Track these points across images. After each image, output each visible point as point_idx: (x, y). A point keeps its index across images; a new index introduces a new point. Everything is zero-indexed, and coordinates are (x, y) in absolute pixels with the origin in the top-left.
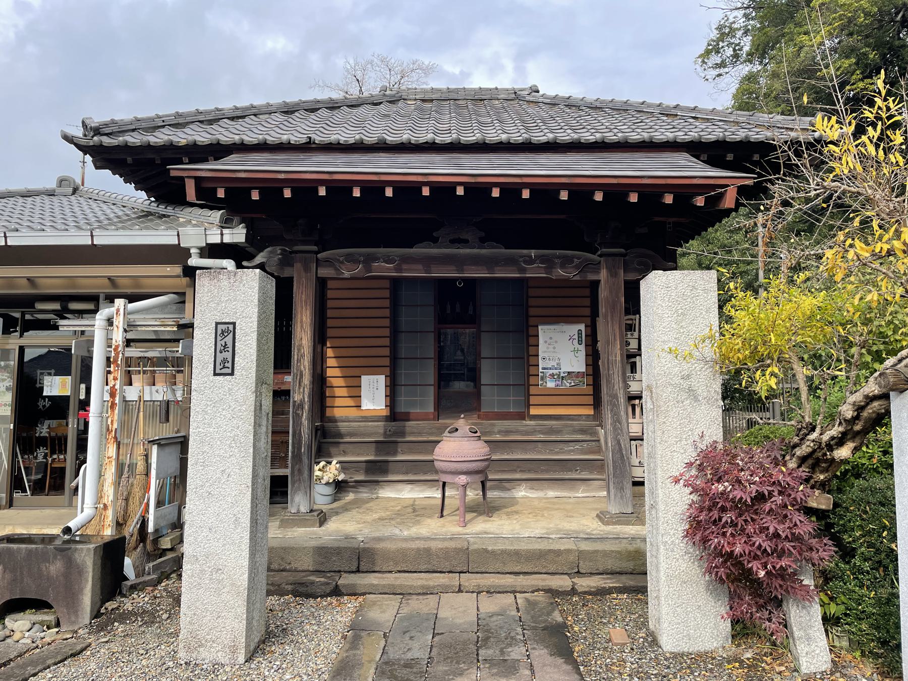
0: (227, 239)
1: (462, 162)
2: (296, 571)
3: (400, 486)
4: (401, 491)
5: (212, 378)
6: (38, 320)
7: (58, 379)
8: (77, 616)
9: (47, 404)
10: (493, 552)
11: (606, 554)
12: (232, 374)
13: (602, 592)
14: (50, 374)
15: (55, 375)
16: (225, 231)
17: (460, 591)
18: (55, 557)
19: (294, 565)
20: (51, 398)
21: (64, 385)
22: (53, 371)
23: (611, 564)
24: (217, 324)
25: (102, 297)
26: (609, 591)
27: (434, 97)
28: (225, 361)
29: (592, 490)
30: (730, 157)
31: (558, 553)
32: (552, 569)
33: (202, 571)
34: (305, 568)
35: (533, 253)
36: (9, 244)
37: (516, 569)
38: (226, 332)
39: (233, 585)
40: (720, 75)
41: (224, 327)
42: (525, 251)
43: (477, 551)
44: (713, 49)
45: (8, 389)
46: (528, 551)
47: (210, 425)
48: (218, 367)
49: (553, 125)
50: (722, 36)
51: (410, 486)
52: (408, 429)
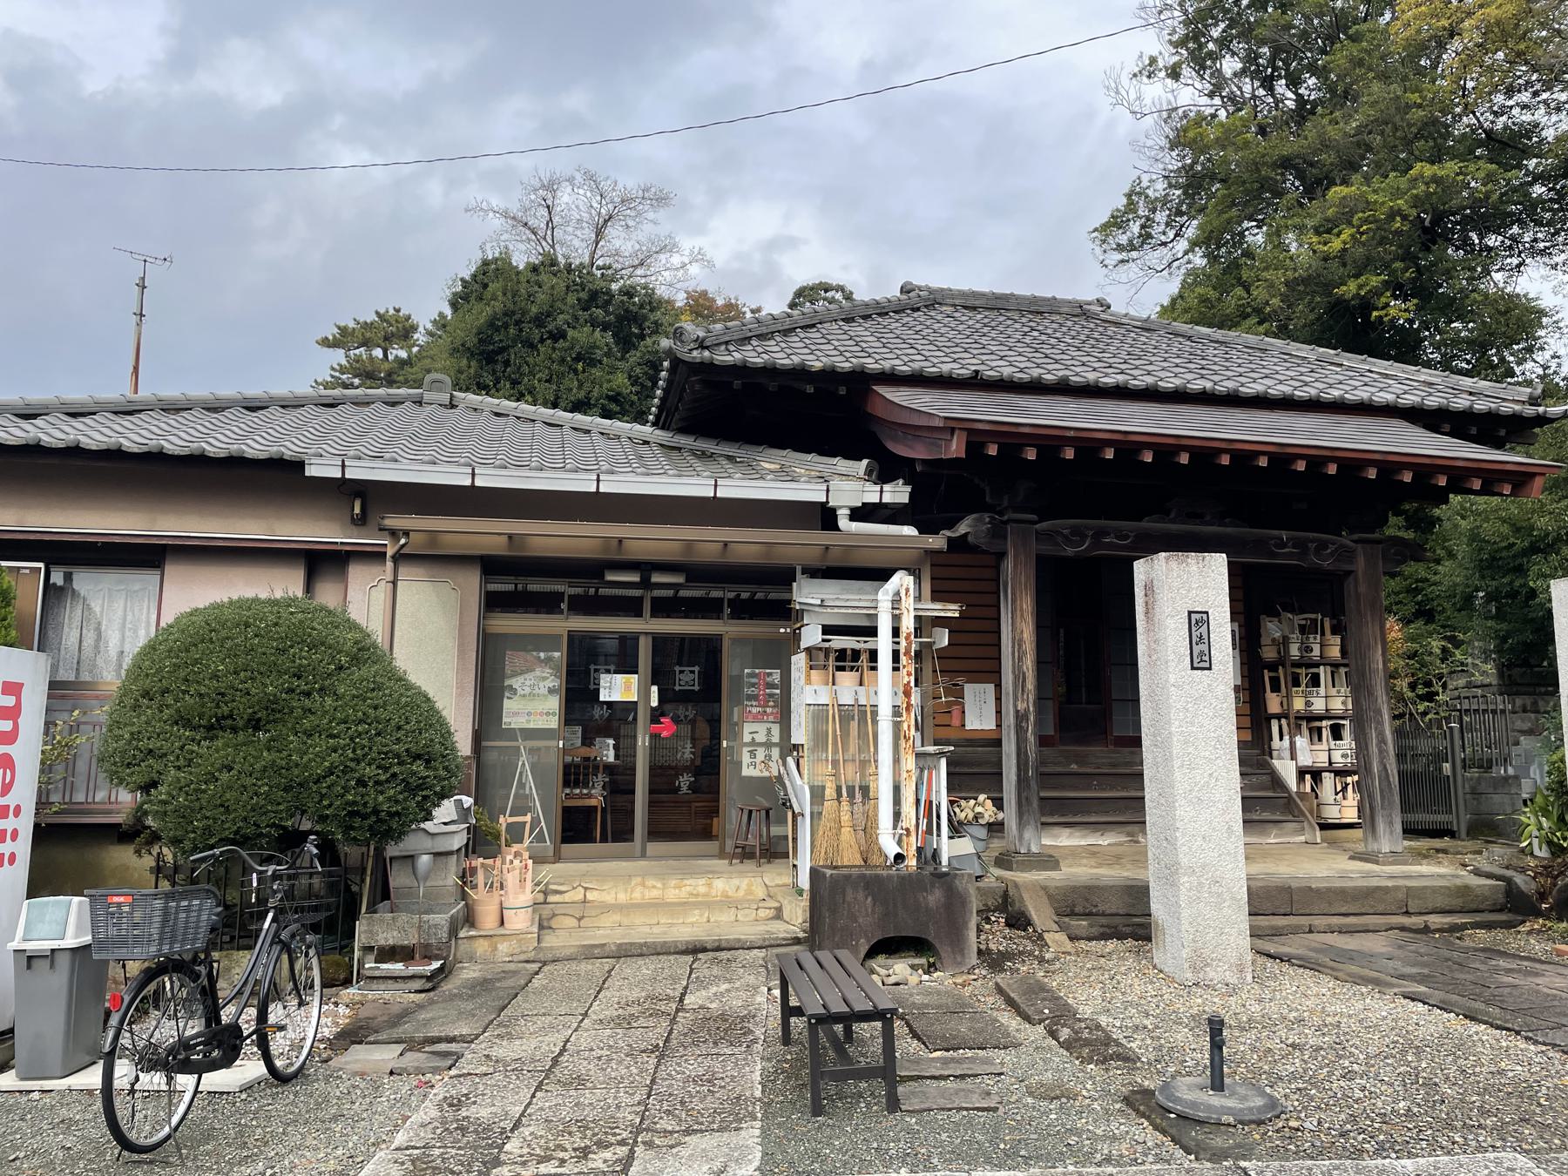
0: (887, 499)
1: (1230, 422)
2: (1103, 915)
3: (1056, 830)
4: (1056, 837)
5: (1190, 672)
6: (526, 593)
7: (620, 678)
8: (963, 955)
9: (606, 713)
10: (1318, 891)
11: (1434, 890)
12: (1210, 669)
13: (1454, 929)
14: (608, 672)
15: (616, 672)
16: (887, 487)
17: (1311, 931)
18: (933, 886)
19: (1101, 908)
20: (610, 704)
21: (628, 688)
22: (612, 668)
23: (1440, 902)
24: (1190, 613)
25: (799, 569)
26: (1463, 927)
27: (977, 303)
28: (1202, 653)
29: (1287, 834)
30: (1474, 431)
31: (1386, 890)
32: (1381, 909)
33: (1200, 884)
34: (1114, 911)
35: (1284, 535)
36: (478, 483)
37: (1343, 910)
38: (1198, 621)
39: (1233, 898)
40: (1122, 261)
41: (1198, 616)
42: (1276, 532)
43: (1300, 889)
44: (1117, 222)
45: (551, 691)
46: (1355, 888)
47: (1192, 724)
48: (1196, 660)
49: (1101, 345)
50: (1131, 207)
51: (1068, 831)
52: (1298, 738)
